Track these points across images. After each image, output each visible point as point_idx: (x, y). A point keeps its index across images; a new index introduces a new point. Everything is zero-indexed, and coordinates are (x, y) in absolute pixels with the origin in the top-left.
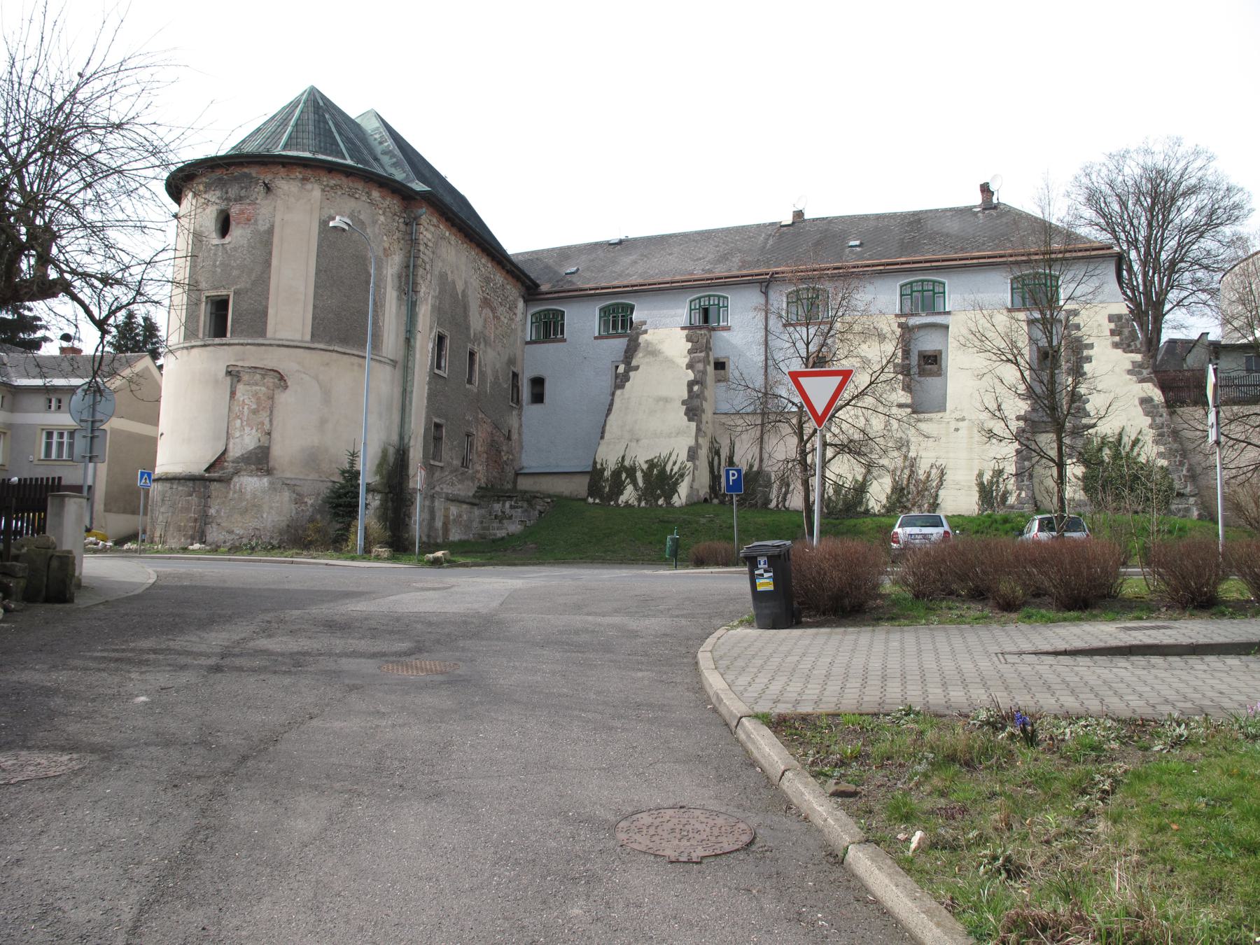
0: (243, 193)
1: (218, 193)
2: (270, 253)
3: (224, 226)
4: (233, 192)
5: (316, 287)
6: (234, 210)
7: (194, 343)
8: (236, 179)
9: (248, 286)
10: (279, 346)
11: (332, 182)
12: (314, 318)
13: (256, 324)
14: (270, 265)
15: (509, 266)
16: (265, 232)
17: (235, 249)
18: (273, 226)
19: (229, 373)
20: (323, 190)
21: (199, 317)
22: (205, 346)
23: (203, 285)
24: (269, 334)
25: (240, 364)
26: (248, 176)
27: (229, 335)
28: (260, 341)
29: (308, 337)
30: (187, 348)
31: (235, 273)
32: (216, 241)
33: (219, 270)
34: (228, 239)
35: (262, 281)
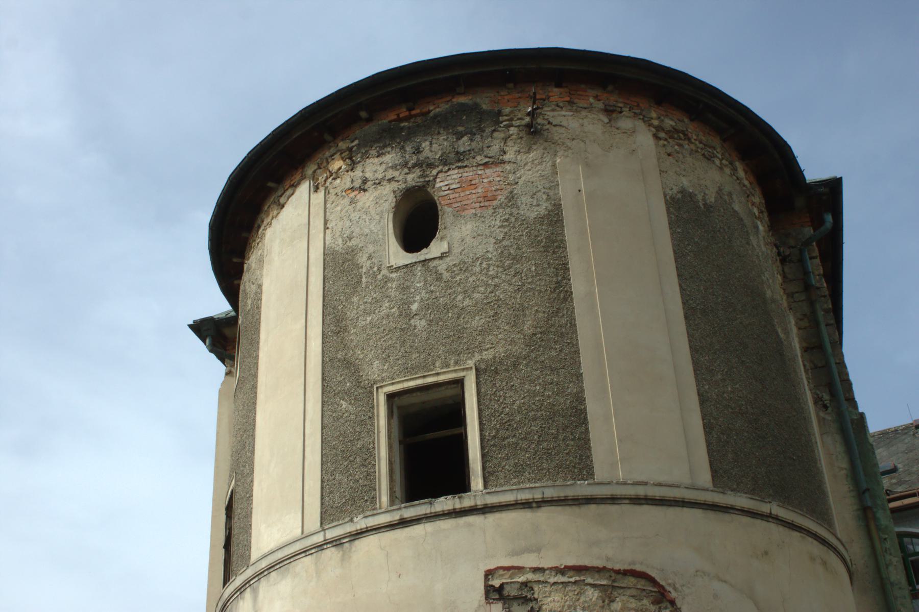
0: (464, 144)
1: (391, 157)
2: (565, 267)
3: (417, 223)
4: (433, 147)
5: (694, 349)
6: (445, 184)
7: (361, 523)
8: (444, 122)
9: (519, 349)
10: (636, 501)
11: (669, 123)
12: (708, 428)
13: (557, 446)
14: (568, 296)
15: (673, 503)
16: (540, 219)
17: (463, 267)
18: (558, 207)
19: (494, 593)
20: (656, 137)
21: (370, 452)
22: (403, 523)
23: (374, 369)
24: (601, 472)
25: (530, 561)
26: (474, 109)
27: (477, 482)
28: (583, 489)
29: (705, 477)
30: (337, 542)
31: (478, 322)
32: (397, 256)
33: (420, 324)
34: (435, 248)
35: (556, 335)
